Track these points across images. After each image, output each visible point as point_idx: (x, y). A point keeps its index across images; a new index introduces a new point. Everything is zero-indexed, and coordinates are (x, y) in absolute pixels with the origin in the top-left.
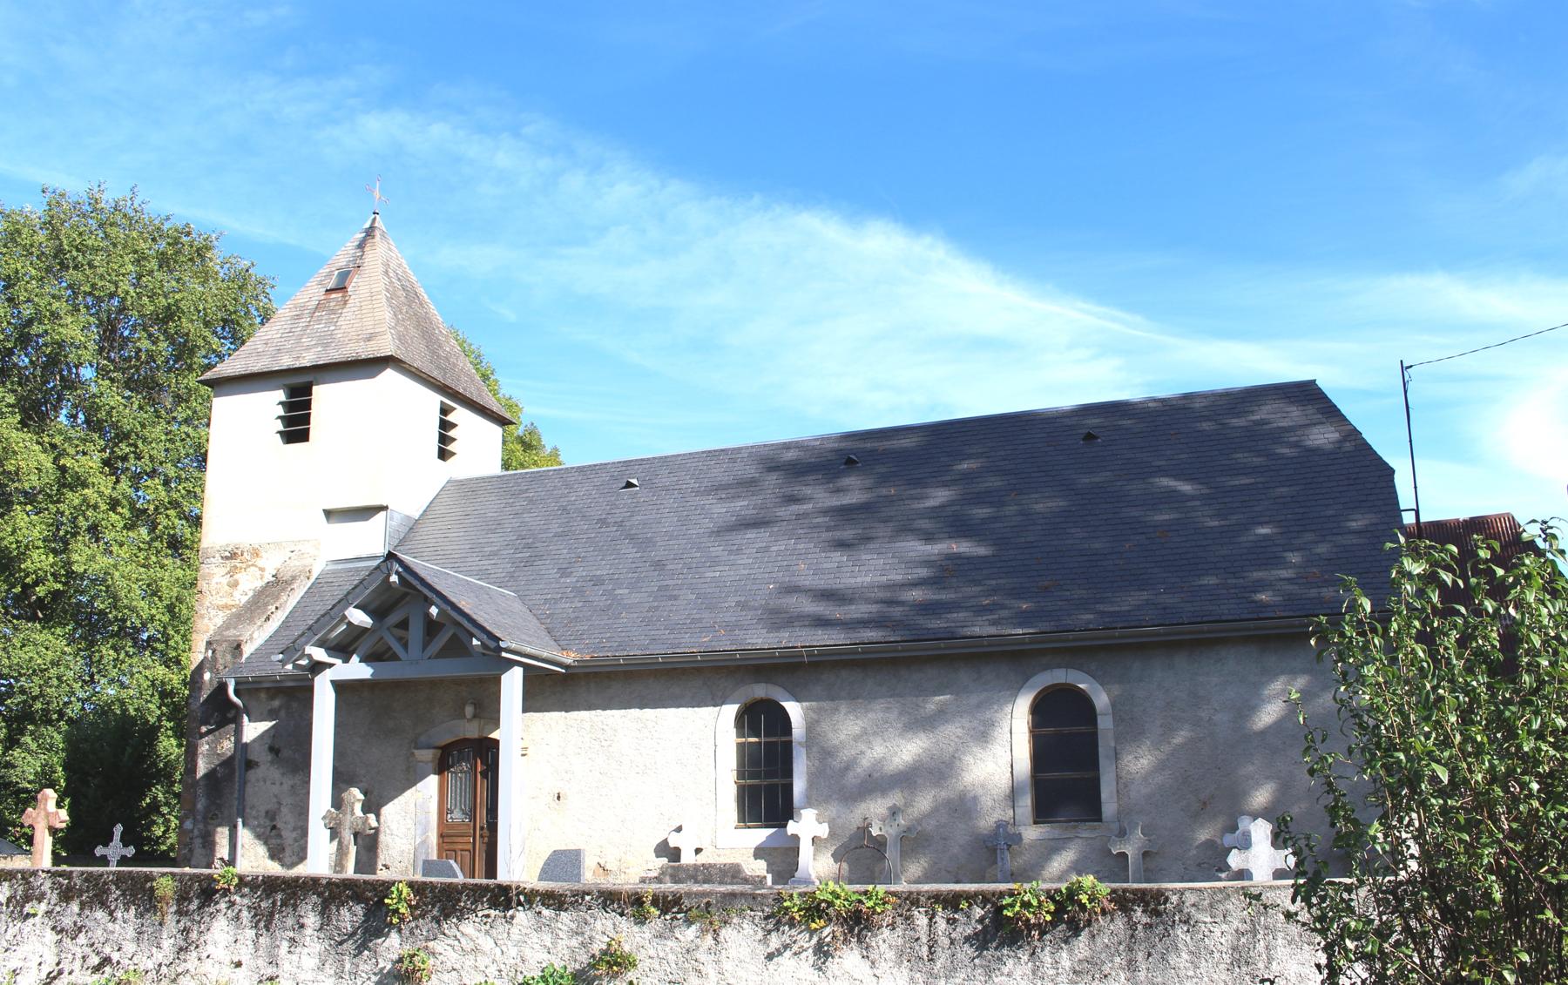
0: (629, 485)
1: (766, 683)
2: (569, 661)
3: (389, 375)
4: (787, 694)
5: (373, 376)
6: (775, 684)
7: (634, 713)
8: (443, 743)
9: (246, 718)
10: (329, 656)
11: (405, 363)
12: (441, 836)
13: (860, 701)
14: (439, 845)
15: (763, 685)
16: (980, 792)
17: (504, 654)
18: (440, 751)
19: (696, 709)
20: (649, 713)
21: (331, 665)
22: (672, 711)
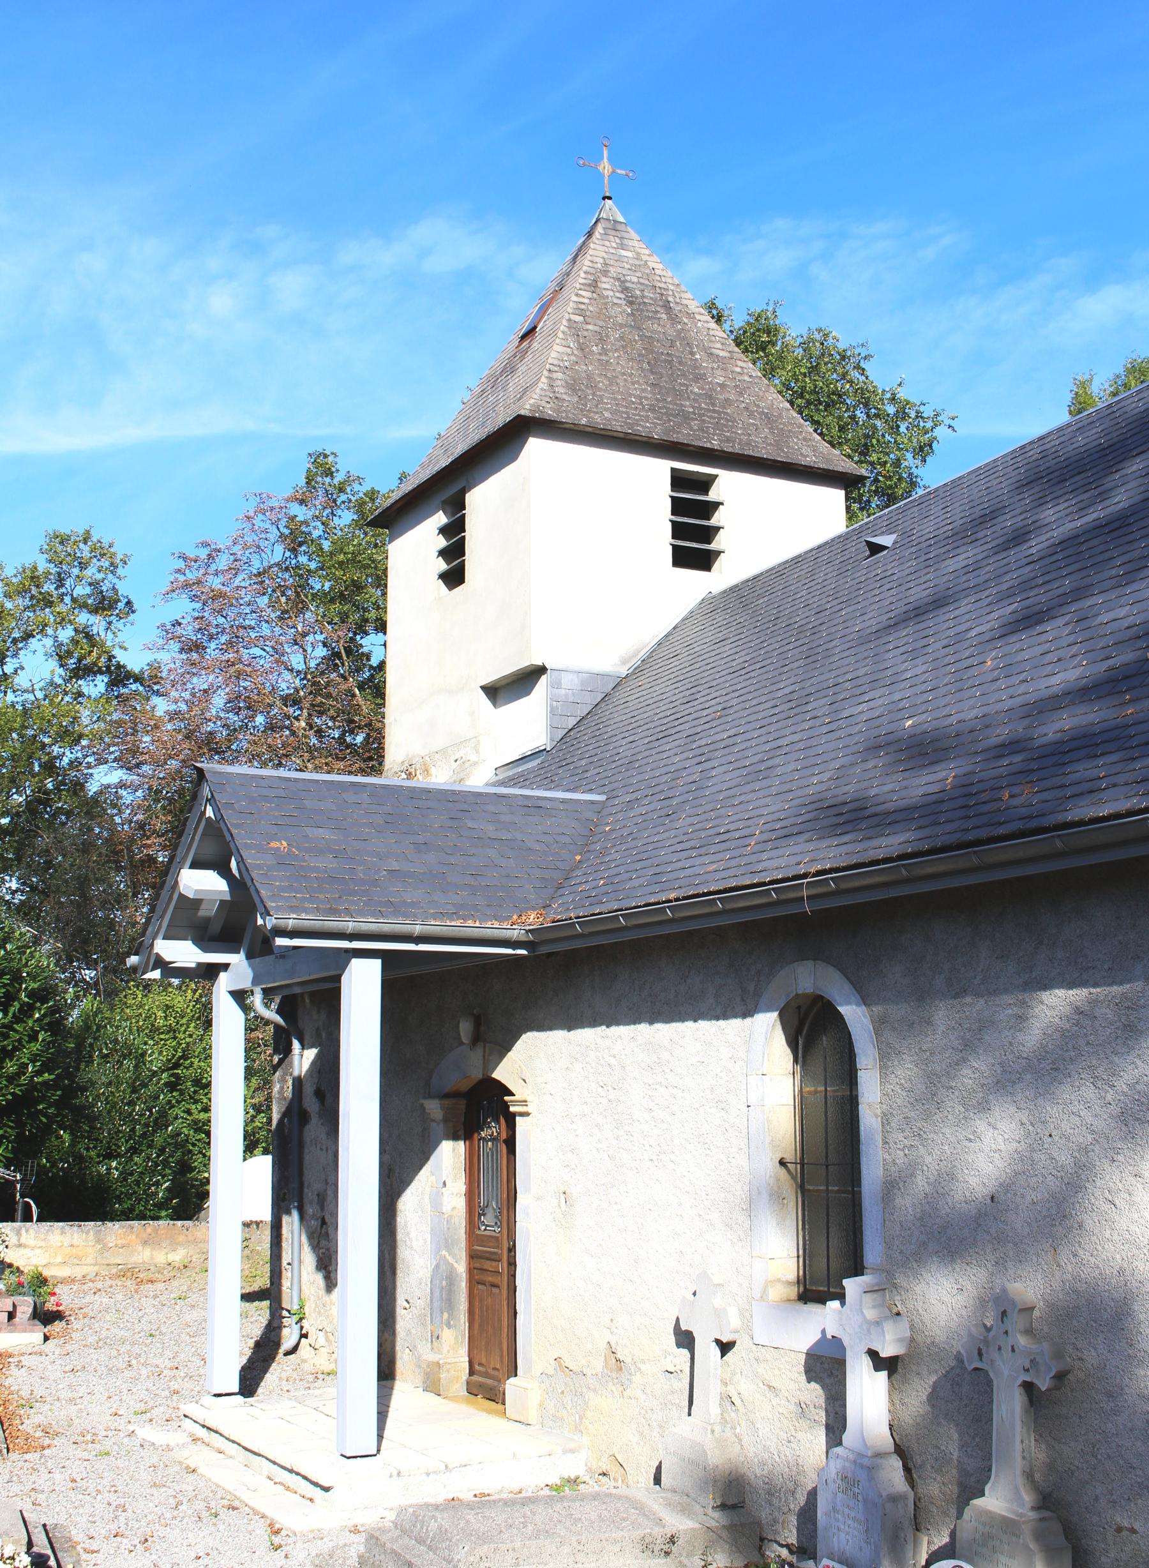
0: (875, 549)
1: (815, 960)
2: (516, 933)
3: (535, 447)
4: (847, 986)
5: (515, 458)
6: (828, 961)
7: (643, 1030)
8: (465, 1086)
9: (296, 1045)
10: (205, 949)
11: (561, 423)
12: (473, 1256)
13: (968, 999)
14: (471, 1271)
15: (810, 963)
16: (745, 1470)
17: (280, 941)
18: (462, 1104)
19: (721, 1023)
20: (662, 1031)
21: (225, 967)
22: (687, 1028)
